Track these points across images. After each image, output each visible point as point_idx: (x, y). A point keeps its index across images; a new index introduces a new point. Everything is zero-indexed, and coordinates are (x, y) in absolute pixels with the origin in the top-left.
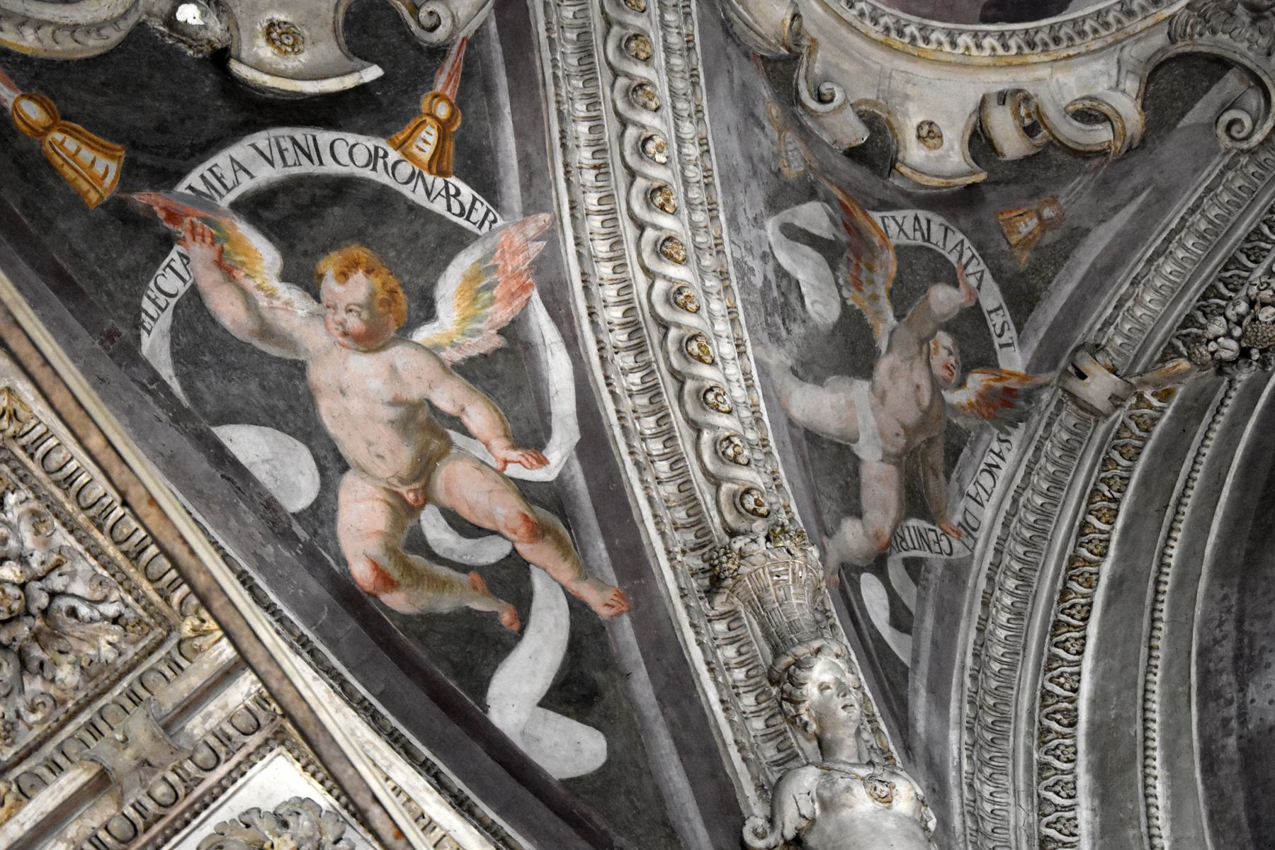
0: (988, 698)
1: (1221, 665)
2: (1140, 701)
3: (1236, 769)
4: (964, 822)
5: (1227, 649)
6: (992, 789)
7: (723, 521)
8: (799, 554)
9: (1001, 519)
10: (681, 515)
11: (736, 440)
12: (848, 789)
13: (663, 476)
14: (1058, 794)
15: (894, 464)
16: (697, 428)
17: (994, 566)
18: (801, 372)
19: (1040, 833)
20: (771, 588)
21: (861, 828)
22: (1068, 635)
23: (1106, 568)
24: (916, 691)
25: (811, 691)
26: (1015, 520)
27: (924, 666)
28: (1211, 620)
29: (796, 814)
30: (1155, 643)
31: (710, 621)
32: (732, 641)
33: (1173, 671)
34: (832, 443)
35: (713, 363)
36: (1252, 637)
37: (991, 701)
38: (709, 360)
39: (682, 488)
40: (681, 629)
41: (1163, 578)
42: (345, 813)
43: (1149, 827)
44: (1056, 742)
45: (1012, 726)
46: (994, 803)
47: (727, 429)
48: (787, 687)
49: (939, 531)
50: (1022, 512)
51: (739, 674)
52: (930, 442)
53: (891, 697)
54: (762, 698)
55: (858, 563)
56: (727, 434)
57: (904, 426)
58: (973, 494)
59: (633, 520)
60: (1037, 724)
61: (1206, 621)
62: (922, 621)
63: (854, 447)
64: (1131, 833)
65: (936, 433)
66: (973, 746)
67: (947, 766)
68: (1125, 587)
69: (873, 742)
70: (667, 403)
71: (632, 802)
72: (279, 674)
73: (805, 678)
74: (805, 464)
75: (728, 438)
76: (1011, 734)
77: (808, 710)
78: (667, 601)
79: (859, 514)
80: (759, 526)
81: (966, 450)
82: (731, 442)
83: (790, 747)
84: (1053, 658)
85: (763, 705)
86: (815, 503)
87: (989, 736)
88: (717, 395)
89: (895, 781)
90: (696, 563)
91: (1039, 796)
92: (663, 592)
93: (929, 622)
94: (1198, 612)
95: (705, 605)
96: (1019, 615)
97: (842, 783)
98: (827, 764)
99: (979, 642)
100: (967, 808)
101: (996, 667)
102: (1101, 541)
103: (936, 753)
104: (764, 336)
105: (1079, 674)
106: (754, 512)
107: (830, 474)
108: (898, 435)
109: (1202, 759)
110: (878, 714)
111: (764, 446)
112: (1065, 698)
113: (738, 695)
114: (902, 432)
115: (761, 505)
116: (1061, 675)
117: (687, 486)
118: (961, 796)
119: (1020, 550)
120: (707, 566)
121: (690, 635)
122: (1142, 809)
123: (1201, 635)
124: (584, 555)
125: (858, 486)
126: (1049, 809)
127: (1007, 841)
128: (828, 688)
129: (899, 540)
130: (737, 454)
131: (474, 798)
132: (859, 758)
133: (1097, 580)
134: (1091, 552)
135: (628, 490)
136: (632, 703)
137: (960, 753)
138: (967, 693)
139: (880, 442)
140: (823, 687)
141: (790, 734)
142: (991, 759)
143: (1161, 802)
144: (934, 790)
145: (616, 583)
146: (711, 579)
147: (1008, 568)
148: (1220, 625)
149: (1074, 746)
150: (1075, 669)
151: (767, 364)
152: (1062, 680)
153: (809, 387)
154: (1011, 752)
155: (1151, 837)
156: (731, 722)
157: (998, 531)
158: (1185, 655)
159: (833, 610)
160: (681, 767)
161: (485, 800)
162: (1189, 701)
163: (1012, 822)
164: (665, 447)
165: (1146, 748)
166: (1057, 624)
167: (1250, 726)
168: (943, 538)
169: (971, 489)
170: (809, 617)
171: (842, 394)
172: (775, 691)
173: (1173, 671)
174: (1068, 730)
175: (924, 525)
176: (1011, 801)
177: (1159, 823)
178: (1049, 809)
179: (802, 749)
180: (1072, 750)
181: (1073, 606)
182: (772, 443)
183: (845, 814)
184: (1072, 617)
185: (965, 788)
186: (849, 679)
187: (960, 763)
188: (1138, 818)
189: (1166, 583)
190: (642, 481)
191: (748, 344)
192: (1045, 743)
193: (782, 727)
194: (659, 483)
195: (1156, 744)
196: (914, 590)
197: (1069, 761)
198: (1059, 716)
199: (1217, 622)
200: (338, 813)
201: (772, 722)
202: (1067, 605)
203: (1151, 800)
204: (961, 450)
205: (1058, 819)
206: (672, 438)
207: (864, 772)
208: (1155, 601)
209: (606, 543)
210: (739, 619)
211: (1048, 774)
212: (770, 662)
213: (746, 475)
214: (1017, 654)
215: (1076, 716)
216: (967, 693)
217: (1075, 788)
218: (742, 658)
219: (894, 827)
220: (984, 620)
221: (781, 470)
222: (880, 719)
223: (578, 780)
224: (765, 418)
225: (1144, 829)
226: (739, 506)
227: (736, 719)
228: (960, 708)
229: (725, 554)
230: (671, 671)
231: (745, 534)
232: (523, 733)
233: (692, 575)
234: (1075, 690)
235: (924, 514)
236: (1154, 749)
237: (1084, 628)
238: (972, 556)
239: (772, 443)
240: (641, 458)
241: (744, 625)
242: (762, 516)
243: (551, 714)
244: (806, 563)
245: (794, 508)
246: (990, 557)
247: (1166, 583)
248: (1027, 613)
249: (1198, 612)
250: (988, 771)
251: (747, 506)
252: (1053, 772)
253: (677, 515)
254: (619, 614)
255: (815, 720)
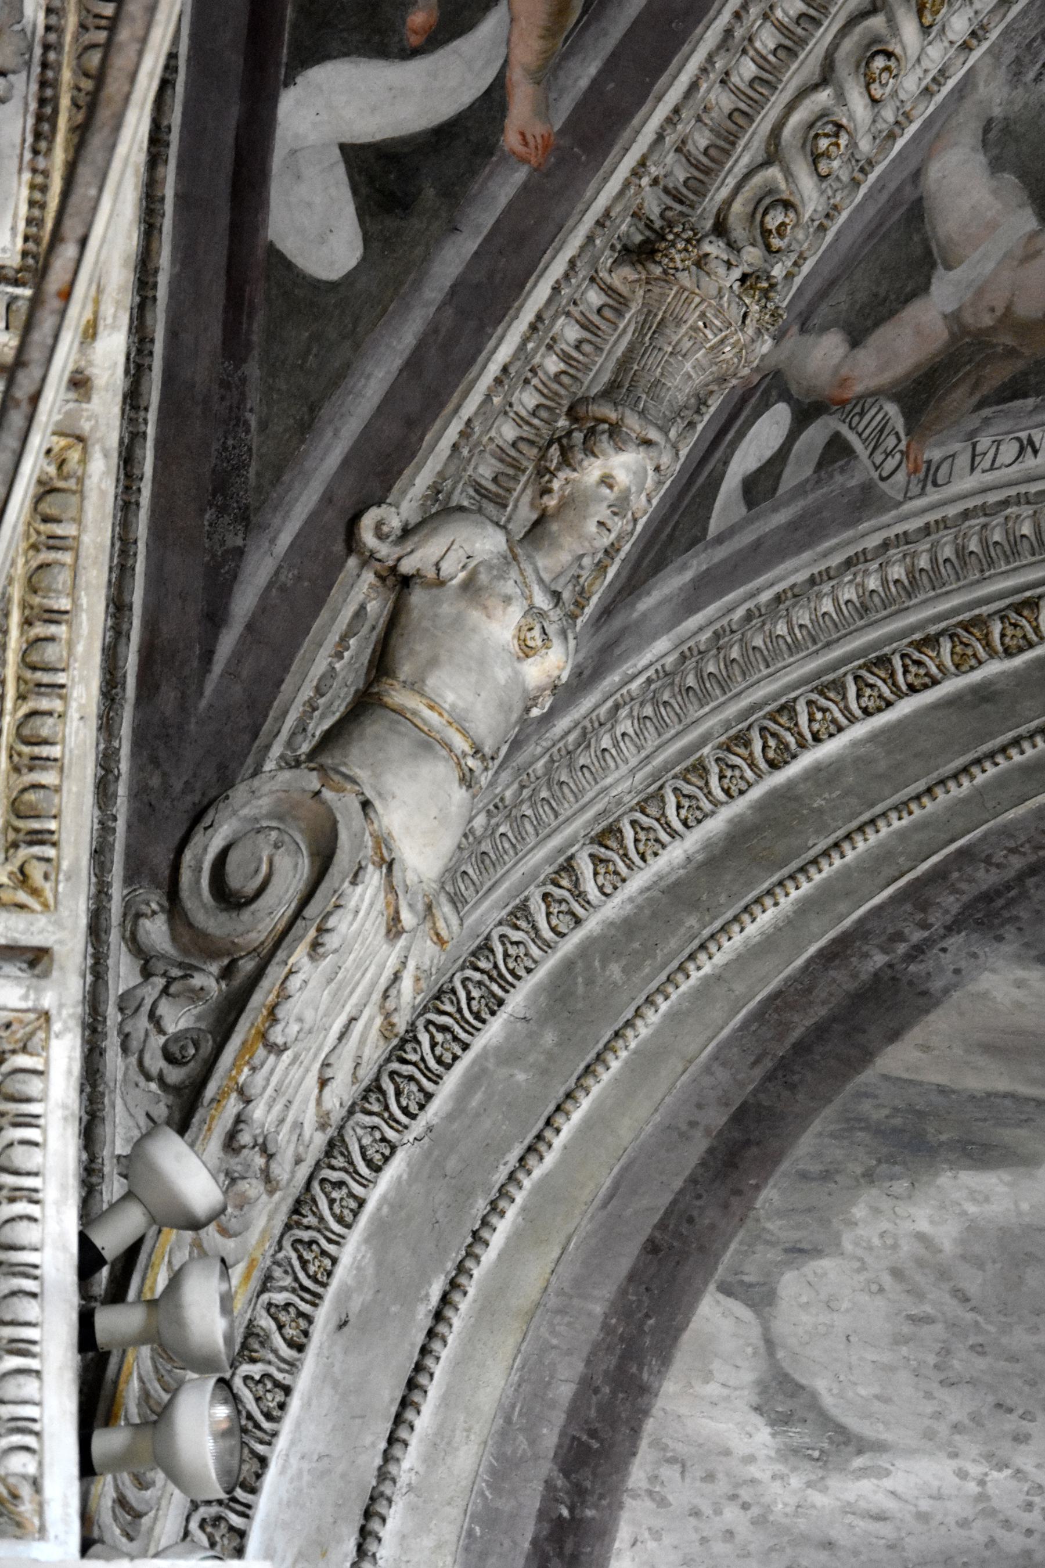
0: (736, 648)
1: (964, 886)
2: (854, 824)
3: (851, 986)
4: (567, 733)
5: (986, 878)
6: (631, 731)
7: (729, 202)
8: (750, 331)
9: (970, 504)
10: (702, 140)
11: (843, 140)
12: (507, 600)
13: (735, 79)
14: (679, 807)
15: (952, 334)
16: (826, 76)
17: (905, 538)
18: (992, 135)
19: (618, 820)
20: (684, 328)
21: (474, 646)
22: (880, 683)
23: (994, 668)
24: (684, 567)
25: (592, 471)
26: (983, 520)
27: (721, 553)
28: (1011, 836)
29: (434, 559)
30: (939, 791)
31: (592, 280)
32: (586, 325)
33: (918, 837)
34: (925, 242)
35: (926, 29)
36: (1024, 895)
37: (735, 653)
38: (928, 19)
39: (736, 115)
40: (557, 251)
41: (1026, 745)
42: (38, 51)
43: (712, 937)
44: (738, 761)
45: (722, 699)
46: (616, 745)
47: (851, 118)
48: (578, 437)
49: (903, 446)
50: (999, 519)
51: (553, 365)
52: (1011, 353)
53: (657, 547)
54: (544, 414)
55: (794, 390)
56: (844, 121)
57: (1008, 308)
58: (979, 449)
59: (652, 84)
60: (745, 724)
61: (1006, 831)
62: (775, 509)
63: (940, 270)
64: (692, 921)
65: (1027, 352)
66: (666, 675)
67: (620, 667)
68: (987, 707)
69: (585, 574)
70: (833, 10)
71: (308, 351)
72: (140, 33)
73: (604, 453)
74: (874, 233)
75: (839, 127)
76: (712, 705)
77: (567, 481)
78: (580, 207)
79: (855, 341)
80: (752, 256)
81: (1031, 402)
82: (837, 135)
83: (509, 491)
84: (839, 686)
85: (536, 421)
86: (832, 284)
87: (691, 681)
88: (887, 69)
89: (557, 643)
90: (653, 209)
91: (661, 787)
92: (588, 194)
93: (781, 517)
94: (1011, 815)
95: (607, 259)
96: (864, 609)
97: (509, 587)
98: (519, 551)
99: (796, 590)
100: (587, 723)
101: (781, 629)
102: (1024, 637)
103: (628, 642)
104: (1010, 53)
105: (840, 729)
106: (766, 233)
107: (883, 270)
108: (992, 310)
109: (834, 941)
110: (622, 554)
111: (862, 170)
112: (800, 734)
113: (527, 381)
114: (999, 312)
115: (781, 235)
116: (824, 710)
117: (741, 121)
118: (597, 706)
119: (948, 552)
120: (658, 224)
121: (558, 269)
122: (729, 915)
123: (984, 837)
124: (566, 56)
125: (892, 313)
126: (653, 811)
127: (583, 791)
128: (611, 487)
129: (858, 409)
130: (826, 155)
131: (173, 152)
132: (555, 579)
133: (972, 668)
134: (1003, 635)
135: (686, 48)
136: (427, 258)
137: (646, 668)
138: (725, 622)
139: (969, 295)
140: (607, 481)
141: (523, 479)
142: (665, 703)
143: (751, 929)
144: (580, 674)
145: (556, 128)
146: (646, 241)
147: (914, 555)
148: (1013, 851)
149: (750, 785)
150: (843, 721)
151: (975, 86)
152: (819, 716)
153: (981, 158)
154: (689, 720)
155: (703, 947)
156: (488, 398)
157: (952, 511)
158: (947, 837)
159: (712, 410)
160: (391, 378)
161: (179, 166)
162: (895, 879)
163: (609, 781)
164: (774, 52)
165: (802, 870)
166: (884, 661)
167: (912, 968)
168: (898, 456)
169: (984, 442)
170: (681, 398)
171: (999, 206)
172: (563, 422)
173: (918, 837)
174: (763, 765)
175: (899, 423)
176: (633, 762)
177: (726, 944)
178: (653, 811)
179: (516, 506)
180: (743, 786)
181: (919, 663)
182: (872, 177)
183: (475, 615)
184: (906, 671)
185: (610, 703)
186: (639, 502)
187: (635, 677)
188: (714, 918)
189: (1022, 752)
190: (710, 59)
191: (986, 45)
192: (729, 750)
193: (525, 463)
194: (722, 82)
195: (817, 878)
196: (808, 471)
197: (727, 792)
198: (772, 743)
199: (1011, 844)
200: (30, 49)
201: (522, 446)
202: (916, 656)
203: (746, 918)
204: (1025, 396)
205: (648, 829)
206: (792, 53)
207: (542, 601)
208: (991, 756)
209: (601, 72)
210: (620, 314)
211: (694, 780)
212: (594, 391)
213: (807, 182)
214: (814, 642)
215: (786, 763)
216: (725, 622)
217: (699, 821)
218: (575, 354)
219: (503, 682)
220: (828, 575)
221: (844, 215)
222: (618, 562)
223: (288, 265)
224: (900, 143)
225: (706, 933)
226: (761, 210)
227: (496, 400)
228: (701, 629)
229: (688, 241)
230: (498, 277)
231: (731, 245)
232: (293, 152)
233: (634, 215)
234: (817, 739)
235: (911, 415)
236: (809, 879)
237: (900, 695)
238: (900, 504)
239: (872, 177)
240: (739, 33)
241: (615, 326)
242: (768, 247)
243: (341, 170)
244: (745, 346)
245: (806, 268)
246: (913, 525)
247: (1022, 752)
248: (874, 616)
249: (1011, 815)
250: (648, 711)
251: (768, 218)
252: (701, 783)
253: (697, 136)
254: (523, 160)
255: (562, 498)
